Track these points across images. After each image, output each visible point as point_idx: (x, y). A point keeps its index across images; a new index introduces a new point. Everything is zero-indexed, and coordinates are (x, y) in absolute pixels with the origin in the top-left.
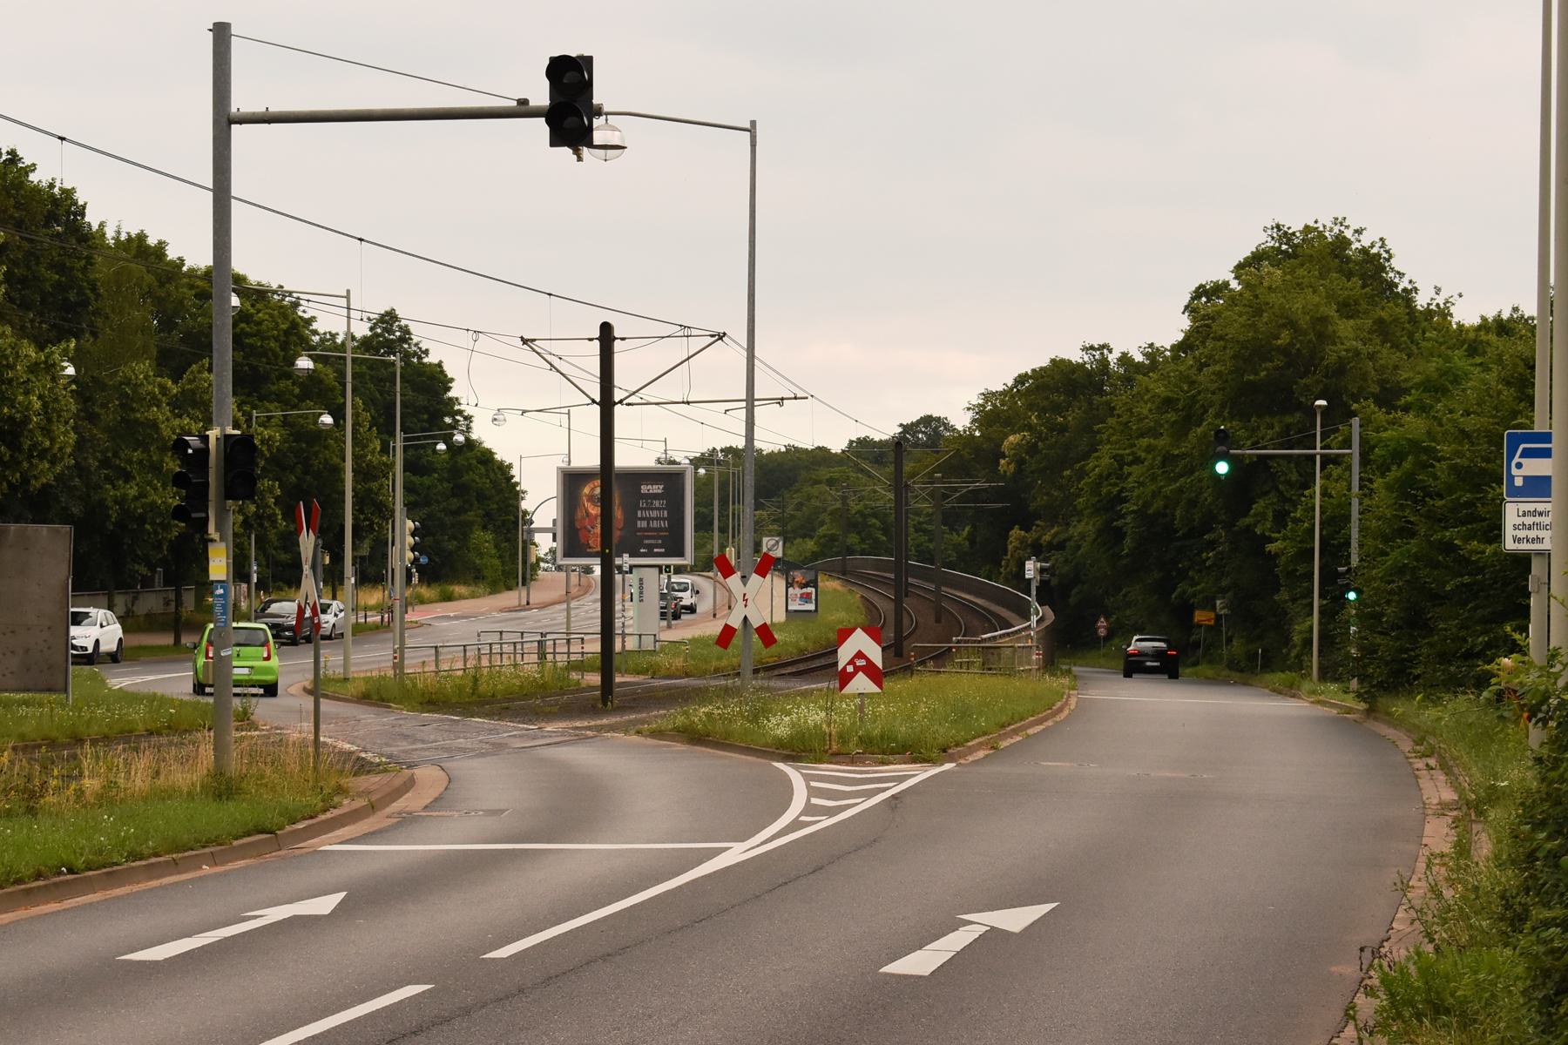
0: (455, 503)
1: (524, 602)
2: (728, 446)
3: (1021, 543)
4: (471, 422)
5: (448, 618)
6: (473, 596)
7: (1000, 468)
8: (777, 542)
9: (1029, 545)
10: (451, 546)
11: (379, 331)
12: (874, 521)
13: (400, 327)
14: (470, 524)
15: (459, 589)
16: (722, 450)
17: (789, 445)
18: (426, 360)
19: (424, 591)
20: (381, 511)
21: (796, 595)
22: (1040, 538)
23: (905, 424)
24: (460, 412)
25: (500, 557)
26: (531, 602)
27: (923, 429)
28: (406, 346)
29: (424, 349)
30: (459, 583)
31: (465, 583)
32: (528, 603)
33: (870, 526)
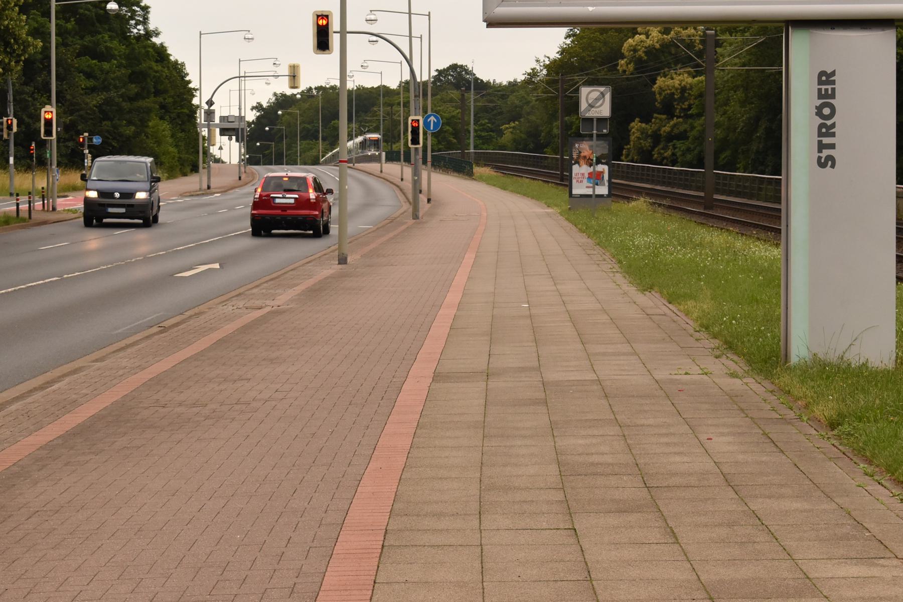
0: (133, 89)
2: (320, 85)
3: (642, 133)
7: (619, 68)
8: (603, 94)
9: (649, 136)
12: (448, 128)
14: (149, 111)
16: (316, 88)
17: (359, 85)
21: (583, 174)
22: (659, 130)
23: (440, 69)
25: (177, 146)
26: (212, 186)
27: (451, 73)
32: (209, 188)
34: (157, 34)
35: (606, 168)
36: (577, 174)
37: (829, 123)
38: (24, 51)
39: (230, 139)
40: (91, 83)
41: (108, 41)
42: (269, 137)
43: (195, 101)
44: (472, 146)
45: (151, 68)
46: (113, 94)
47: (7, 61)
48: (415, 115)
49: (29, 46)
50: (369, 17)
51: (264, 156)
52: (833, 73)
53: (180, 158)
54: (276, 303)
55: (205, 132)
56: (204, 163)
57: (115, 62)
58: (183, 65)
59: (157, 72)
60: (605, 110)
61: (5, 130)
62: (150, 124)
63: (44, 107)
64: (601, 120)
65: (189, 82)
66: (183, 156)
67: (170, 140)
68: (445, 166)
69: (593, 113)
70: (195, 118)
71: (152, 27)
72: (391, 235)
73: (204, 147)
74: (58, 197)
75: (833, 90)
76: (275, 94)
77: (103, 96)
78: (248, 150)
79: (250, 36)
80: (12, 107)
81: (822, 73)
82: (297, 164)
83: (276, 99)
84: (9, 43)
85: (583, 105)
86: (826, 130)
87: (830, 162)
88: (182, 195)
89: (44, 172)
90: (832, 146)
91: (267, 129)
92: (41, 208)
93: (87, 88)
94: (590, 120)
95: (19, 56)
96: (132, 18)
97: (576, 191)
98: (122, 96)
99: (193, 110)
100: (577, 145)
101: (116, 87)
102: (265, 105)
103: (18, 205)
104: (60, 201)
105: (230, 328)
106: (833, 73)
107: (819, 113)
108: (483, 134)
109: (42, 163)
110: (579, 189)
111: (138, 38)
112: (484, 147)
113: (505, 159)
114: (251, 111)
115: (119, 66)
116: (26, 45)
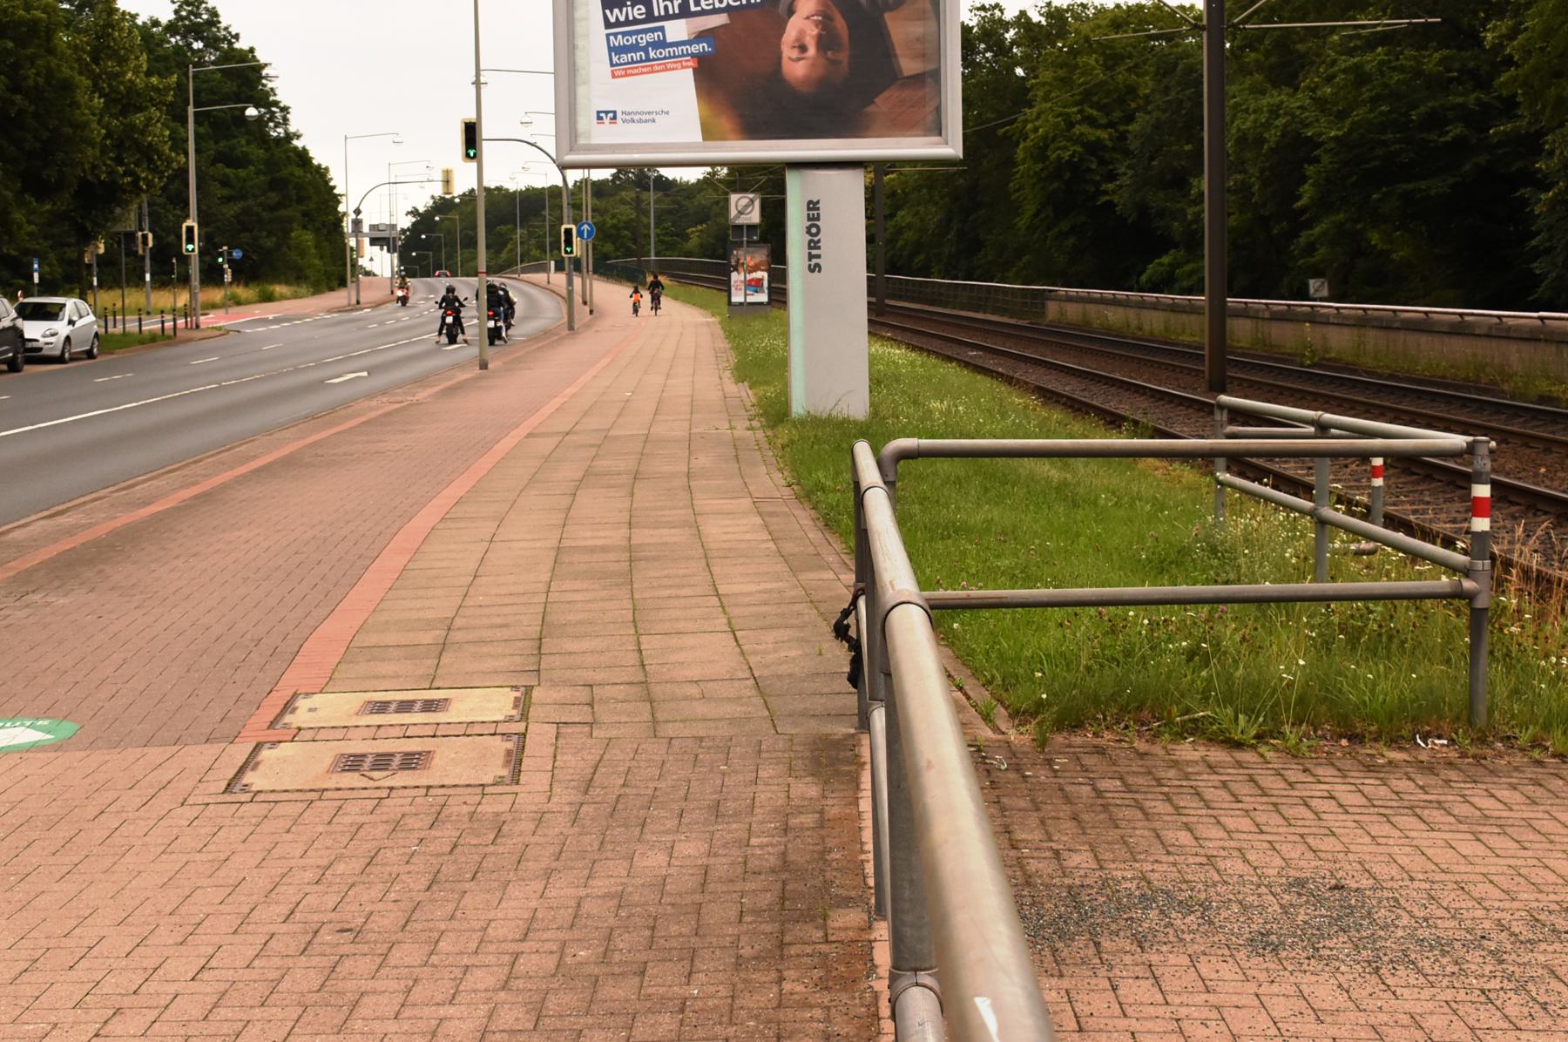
0: (273, 197)
1: (354, 301)
4: (288, 113)
5: (266, 322)
6: (295, 296)
10: (269, 243)
11: (184, 13)
12: (626, 232)
13: (207, 9)
15: (279, 289)
18: (237, 46)
19: (241, 292)
20: (150, 160)
24: (276, 104)
25: (321, 258)
26: (361, 300)
28: (215, 30)
29: (233, 33)
30: (280, 283)
31: (287, 283)
32: (358, 303)
33: (624, 237)
34: (298, 137)
35: (765, 275)
36: (736, 282)
37: (816, 239)
38: (168, 167)
39: (382, 249)
40: (226, 192)
41: (242, 145)
42: (426, 245)
43: (341, 208)
44: (652, 253)
45: (292, 175)
46: (251, 202)
47: (150, 177)
48: (569, 223)
49: (172, 162)
50: (524, 120)
51: (421, 267)
52: (818, 202)
53: (326, 271)
54: (416, 398)
55: (352, 242)
56: (352, 276)
57: (253, 168)
58: (327, 169)
59: (299, 178)
60: (754, 217)
61: (140, 246)
62: (293, 235)
63: (185, 221)
64: (751, 227)
65: (334, 187)
66: (328, 269)
67: (313, 251)
68: (618, 275)
69: (742, 220)
70: (342, 227)
71: (292, 129)
72: (540, 344)
73: (352, 259)
74: (203, 315)
75: (818, 214)
76: (433, 197)
77: (241, 205)
78: (402, 260)
79: (399, 140)
80: (147, 221)
81: (810, 202)
82: (457, 276)
83: (434, 203)
84: (153, 159)
85: (733, 212)
86: (814, 245)
87: (817, 268)
88: (330, 311)
89: (184, 288)
90: (818, 256)
91: (423, 237)
92: (184, 325)
93: (223, 197)
94: (740, 227)
95: (163, 172)
96: (271, 120)
97: (735, 299)
98: (261, 204)
99: (338, 219)
100: (735, 252)
101: (255, 196)
102: (421, 210)
103: (163, 322)
104: (202, 318)
105: (373, 414)
106: (818, 202)
107: (809, 232)
108: (667, 239)
109: (185, 280)
110: (737, 298)
111: (278, 140)
112: (668, 253)
113: (689, 266)
114: (449, 167)
115: (258, 173)
116: (169, 161)
